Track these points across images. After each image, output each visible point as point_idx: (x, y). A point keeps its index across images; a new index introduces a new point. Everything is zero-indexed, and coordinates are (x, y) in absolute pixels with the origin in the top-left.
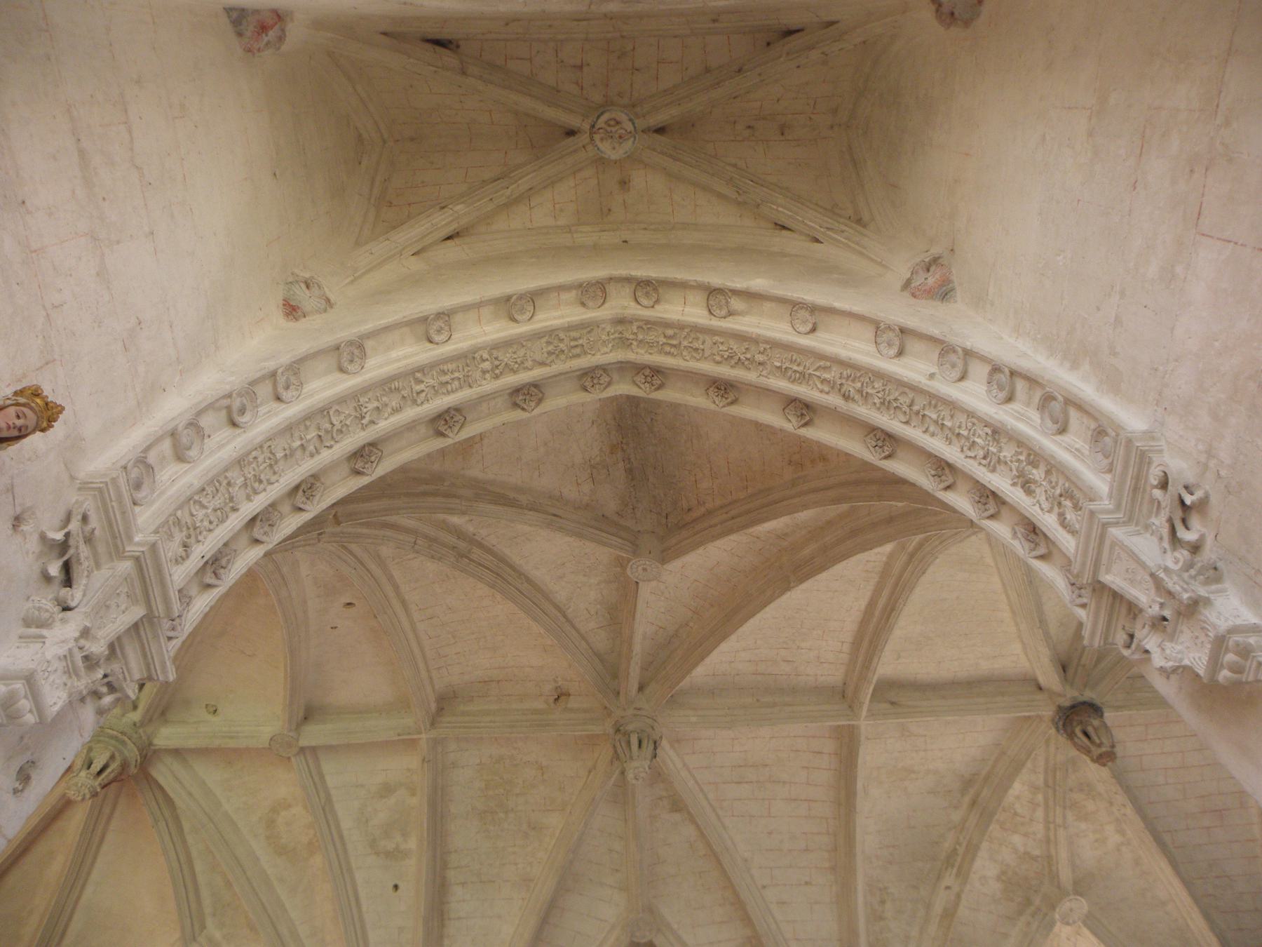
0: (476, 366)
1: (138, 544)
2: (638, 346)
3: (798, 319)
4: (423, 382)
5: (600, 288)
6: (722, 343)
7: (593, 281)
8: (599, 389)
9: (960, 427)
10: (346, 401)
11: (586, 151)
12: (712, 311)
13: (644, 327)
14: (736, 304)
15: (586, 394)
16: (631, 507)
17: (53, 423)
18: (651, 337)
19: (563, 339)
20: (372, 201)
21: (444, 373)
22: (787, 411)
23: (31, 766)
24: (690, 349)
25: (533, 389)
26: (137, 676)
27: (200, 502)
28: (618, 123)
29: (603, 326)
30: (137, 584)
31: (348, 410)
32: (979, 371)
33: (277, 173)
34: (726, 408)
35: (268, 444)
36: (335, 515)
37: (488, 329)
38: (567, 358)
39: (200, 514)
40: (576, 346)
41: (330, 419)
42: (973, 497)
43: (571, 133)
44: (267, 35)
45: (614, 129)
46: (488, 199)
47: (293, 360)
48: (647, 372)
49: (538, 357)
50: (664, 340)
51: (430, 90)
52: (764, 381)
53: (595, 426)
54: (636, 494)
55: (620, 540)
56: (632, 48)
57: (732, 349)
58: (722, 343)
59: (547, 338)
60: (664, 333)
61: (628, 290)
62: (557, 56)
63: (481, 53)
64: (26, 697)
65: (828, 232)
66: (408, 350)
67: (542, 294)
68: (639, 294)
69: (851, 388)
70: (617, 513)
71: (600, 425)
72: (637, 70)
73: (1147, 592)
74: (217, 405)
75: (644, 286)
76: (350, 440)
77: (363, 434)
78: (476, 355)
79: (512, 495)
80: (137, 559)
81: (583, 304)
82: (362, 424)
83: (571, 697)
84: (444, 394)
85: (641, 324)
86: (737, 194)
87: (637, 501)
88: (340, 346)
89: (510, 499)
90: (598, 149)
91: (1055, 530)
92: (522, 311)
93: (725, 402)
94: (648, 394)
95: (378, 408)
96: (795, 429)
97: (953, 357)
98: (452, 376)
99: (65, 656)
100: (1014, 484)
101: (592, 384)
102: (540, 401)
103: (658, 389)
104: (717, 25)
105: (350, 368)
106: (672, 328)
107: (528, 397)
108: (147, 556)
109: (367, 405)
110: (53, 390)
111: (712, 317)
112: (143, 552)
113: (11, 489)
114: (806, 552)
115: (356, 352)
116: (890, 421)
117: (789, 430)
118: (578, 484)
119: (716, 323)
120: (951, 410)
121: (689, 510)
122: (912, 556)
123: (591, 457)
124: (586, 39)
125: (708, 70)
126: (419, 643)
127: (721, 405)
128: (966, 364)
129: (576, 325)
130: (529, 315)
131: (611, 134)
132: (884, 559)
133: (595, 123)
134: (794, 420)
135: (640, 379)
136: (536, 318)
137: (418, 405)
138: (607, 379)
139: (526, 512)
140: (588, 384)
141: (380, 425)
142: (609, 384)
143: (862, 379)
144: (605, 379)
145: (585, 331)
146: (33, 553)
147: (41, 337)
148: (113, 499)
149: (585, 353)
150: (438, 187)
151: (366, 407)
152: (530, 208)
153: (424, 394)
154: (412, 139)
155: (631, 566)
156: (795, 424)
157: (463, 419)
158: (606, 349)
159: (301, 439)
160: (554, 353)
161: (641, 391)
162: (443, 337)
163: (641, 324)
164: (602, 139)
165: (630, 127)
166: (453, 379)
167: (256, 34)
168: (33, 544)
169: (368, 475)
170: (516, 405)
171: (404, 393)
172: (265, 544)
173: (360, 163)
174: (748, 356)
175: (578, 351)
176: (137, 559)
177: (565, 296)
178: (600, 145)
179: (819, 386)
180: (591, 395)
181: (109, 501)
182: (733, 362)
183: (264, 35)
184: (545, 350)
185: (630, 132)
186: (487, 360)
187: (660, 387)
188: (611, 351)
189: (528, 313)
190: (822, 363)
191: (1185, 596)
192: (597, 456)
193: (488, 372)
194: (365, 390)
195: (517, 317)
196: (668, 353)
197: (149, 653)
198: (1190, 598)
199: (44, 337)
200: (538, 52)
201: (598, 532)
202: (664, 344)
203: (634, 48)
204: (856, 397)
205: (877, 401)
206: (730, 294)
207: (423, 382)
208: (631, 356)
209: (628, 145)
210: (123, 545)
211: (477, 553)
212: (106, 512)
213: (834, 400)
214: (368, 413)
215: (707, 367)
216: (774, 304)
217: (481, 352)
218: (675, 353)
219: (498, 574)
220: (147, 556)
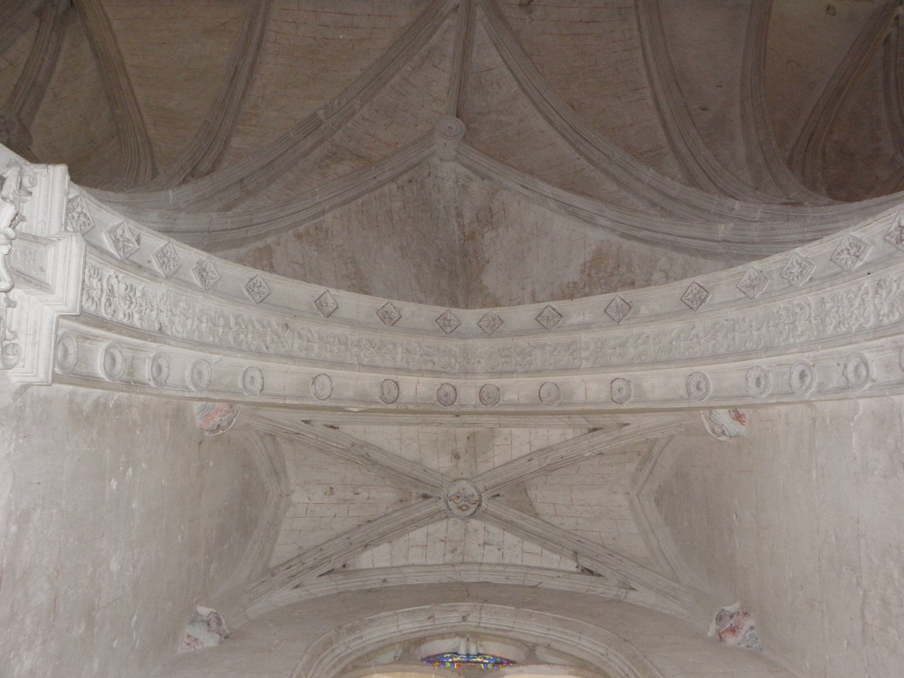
5: (484, 400)
12: (395, 385)
16: (459, 184)
28: (460, 508)
44: (731, 625)
45: (463, 503)
46: (564, 458)
53: (487, 259)
56: (446, 556)
62: (503, 552)
63: (560, 560)
68: (452, 395)
70: (471, 180)
71: (482, 259)
72: (443, 541)
83: (518, 3)
86: (370, 454)
87: (453, 188)
89: (564, 209)
91: (102, 263)
94: (449, 310)
96: (328, 290)
104: (383, 577)
111: (395, 380)
117: (333, 289)
126: (647, 67)
130: (545, 387)
150: (601, 463)
152: (530, 443)
162: (617, 384)
164: (473, 496)
165: (451, 504)
167: (739, 627)
183: (733, 626)
185: (451, 500)
189: (545, 388)
192: (486, 232)
200: (517, 557)
203: (444, 555)
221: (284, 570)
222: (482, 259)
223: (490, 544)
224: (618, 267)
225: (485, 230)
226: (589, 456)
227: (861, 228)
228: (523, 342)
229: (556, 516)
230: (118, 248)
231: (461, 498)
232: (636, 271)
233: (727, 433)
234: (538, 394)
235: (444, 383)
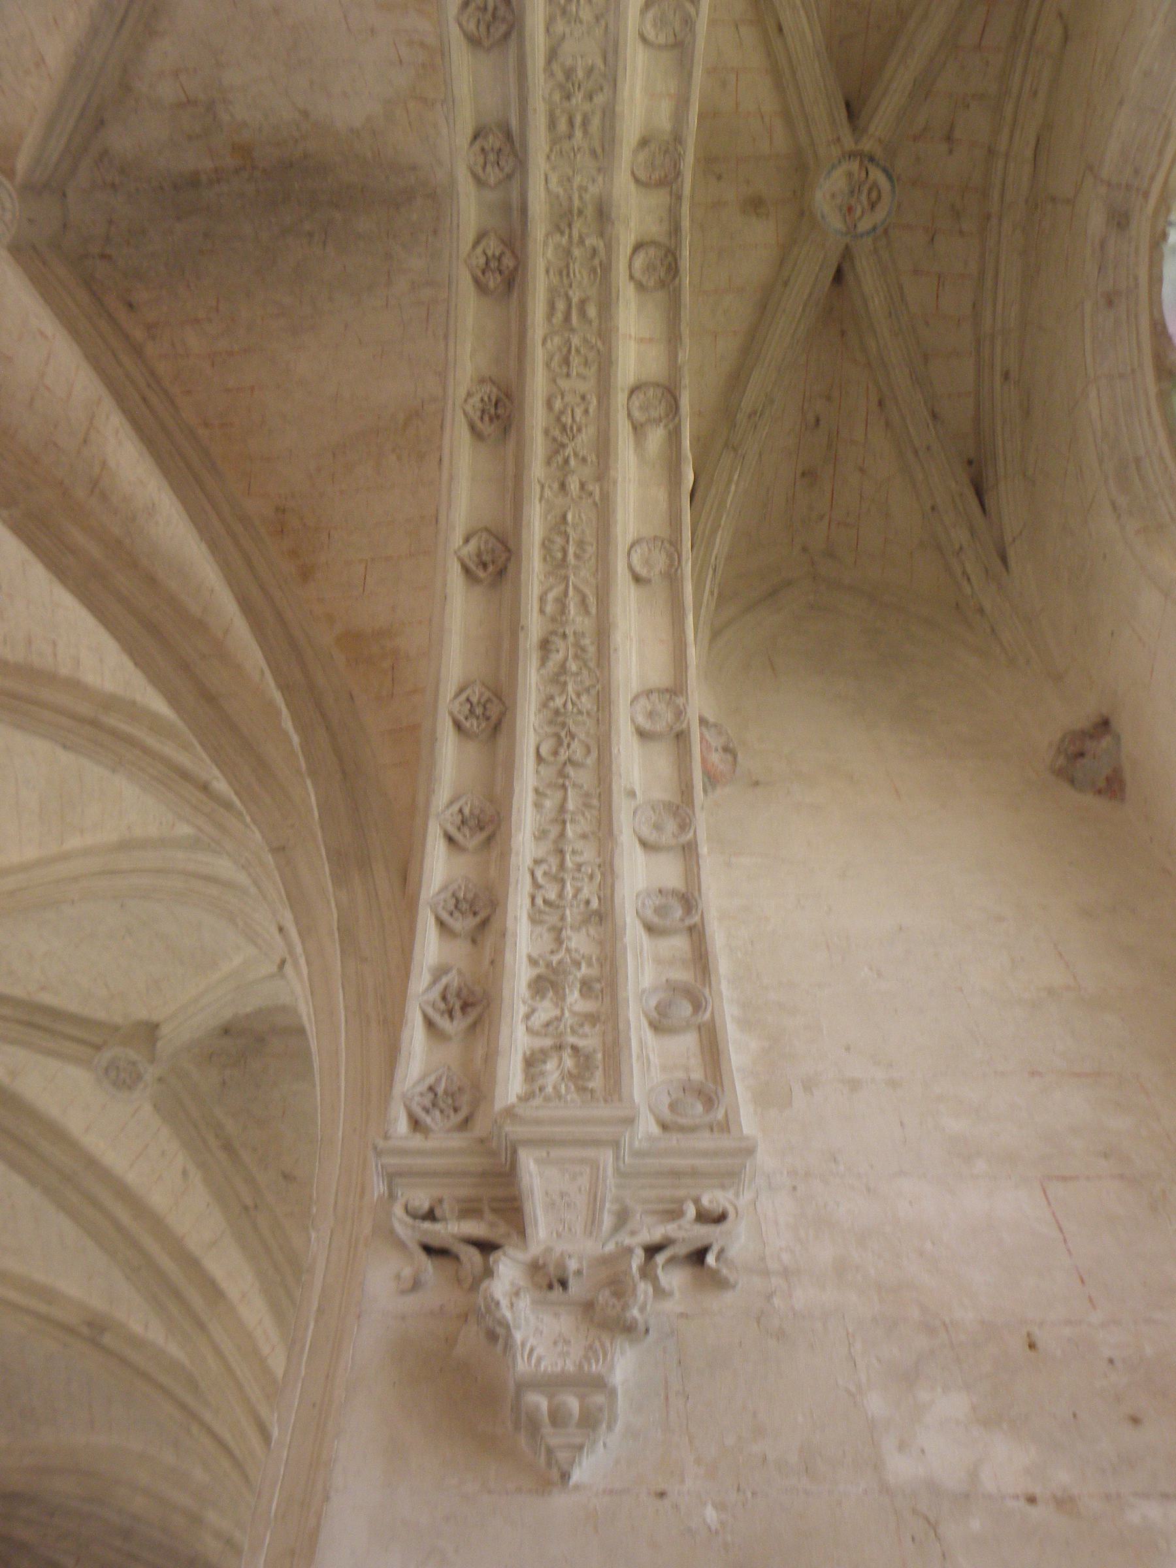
3: (650, 550)
6: (586, 411)
9: (574, 852)
13: (596, 262)
14: (656, 437)
18: (579, 270)
19: (591, 98)
22: (485, 535)
24: (565, 350)
25: (503, 28)
28: (873, 206)
29: (600, 179)
32: (669, 873)
34: (463, 420)
40: (571, 123)
42: (460, 887)
43: (852, 111)
45: (864, 197)
48: (508, 262)
49: (568, 47)
52: (533, 493)
57: (579, 430)
58: (586, 411)
59: (602, 67)
65: (711, 569)
68: (652, 251)
69: (562, 650)
73: (555, 1235)
81: (644, 142)
92: (661, 22)
93: (476, 417)
97: (671, 826)
100: (533, 962)
102: (474, 41)
103: (477, 281)
104: (998, 377)
106: (600, 315)
107: (488, 16)
114: (78, 537)
116: (532, 729)
119: (620, 399)
120: (593, 833)
121: (130, 305)
122: (94, 723)
124: (991, 151)
125: (926, 359)
127: (469, 408)
128: (669, 849)
129: (613, 127)
130: (651, 34)
132: (64, 671)
133: (878, 165)
134: (472, 546)
135: (493, 246)
136: (640, 47)
142: (479, 182)
143: (585, 672)
144: (493, 175)
145: (597, 144)
149: (554, 142)
156: (465, 552)
158: (554, 180)
161: (470, 245)
164: (850, 175)
174: (572, 462)
175: (562, 126)
178: (839, 173)
179: (551, 596)
180: (466, 146)
182: (557, 433)
190: (592, 600)
191: (635, 1312)
196: (552, 307)
198: (635, 1320)
202: (569, 300)
204: (550, 664)
205: (559, 702)
206: (671, 426)
208: (539, 228)
209: (836, 222)
213: (534, 626)
215: (538, 384)
216: (663, 506)
221: (972, 588)
223: (952, 128)
230: (533, 1070)
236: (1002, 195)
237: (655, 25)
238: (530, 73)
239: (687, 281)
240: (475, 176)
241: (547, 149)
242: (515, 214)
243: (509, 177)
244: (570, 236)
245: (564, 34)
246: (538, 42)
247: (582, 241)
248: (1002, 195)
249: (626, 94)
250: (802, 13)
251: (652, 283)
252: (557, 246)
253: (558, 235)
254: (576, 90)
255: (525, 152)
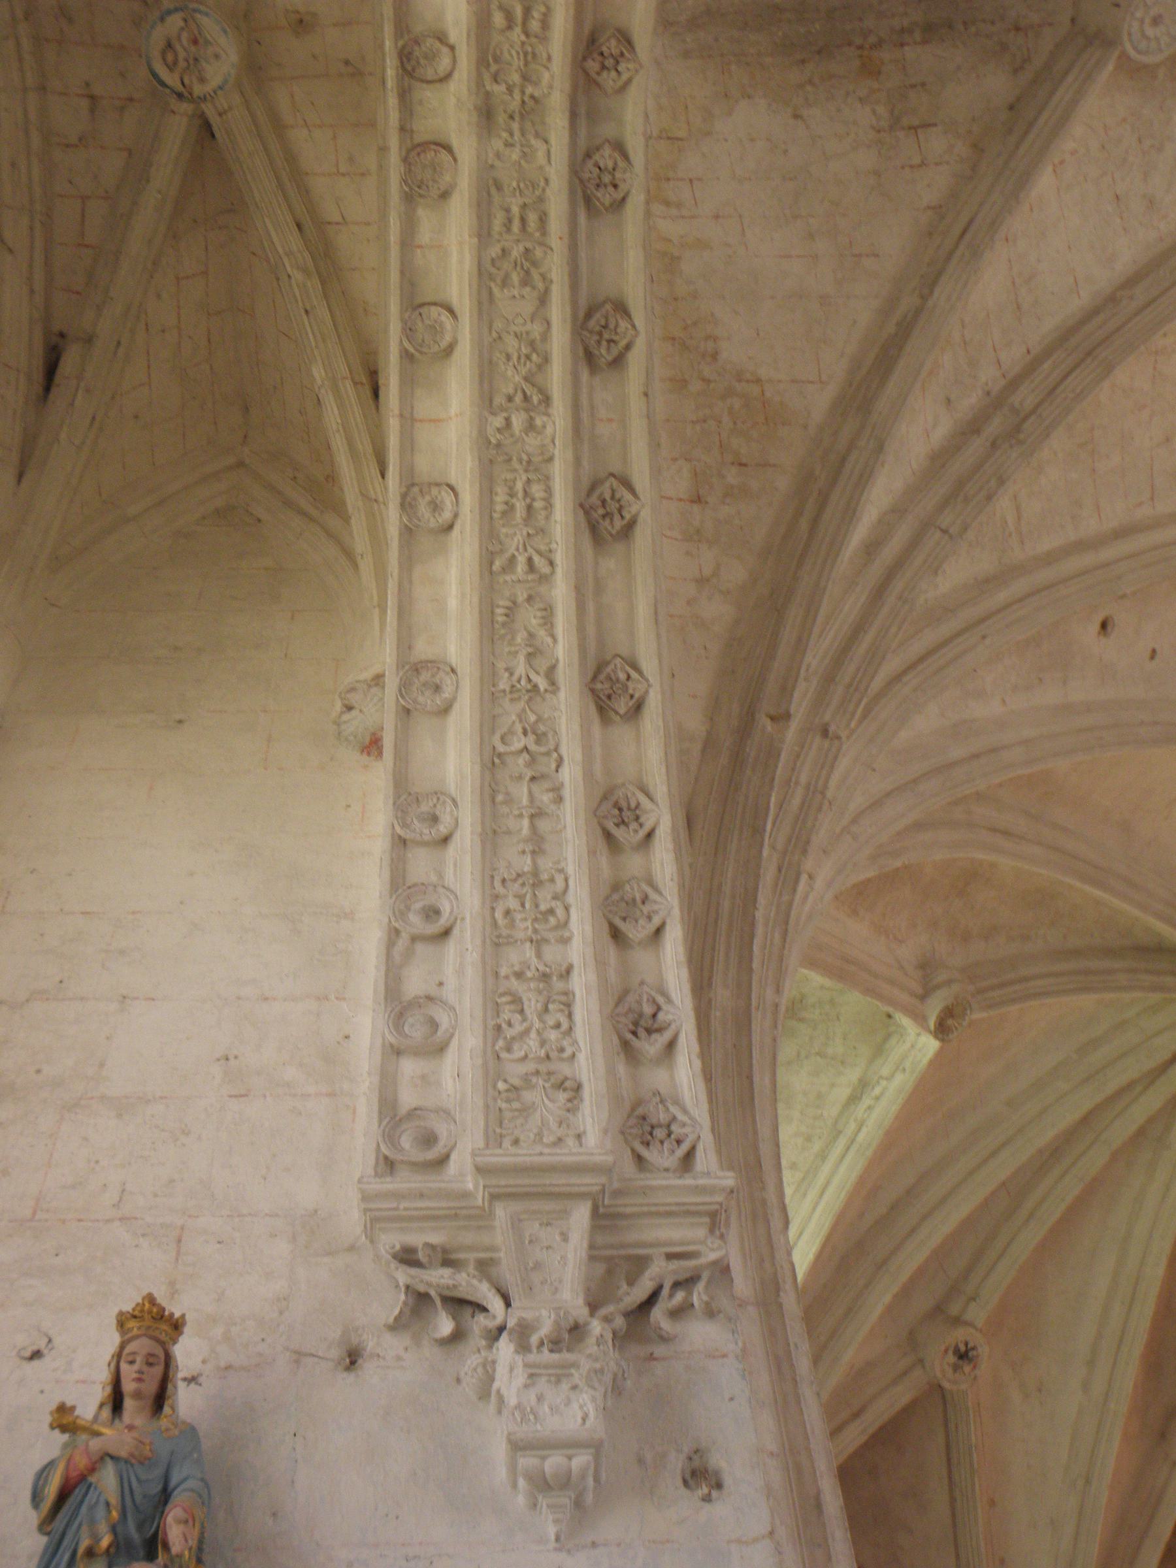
0: (516, 442)
1: (476, 1186)
2: (536, 84)
4: (514, 556)
5: (419, 154)
7: (402, 169)
8: (624, 172)
10: (494, 716)
11: (230, 108)
15: (629, 200)
17: (167, 1313)
19: (503, 250)
20: (314, 513)
21: (510, 508)
23: (701, 1457)
25: (592, 323)
26: (701, 1233)
27: (513, 1038)
28: (169, 45)
30: (535, 1205)
31: (510, 713)
33: (178, 717)
35: (497, 884)
36: (772, 718)
37: (454, 409)
38: (542, 244)
39: (532, 1042)
40: (523, 220)
41: (512, 753)
45: (182, 54)
46: (305, 317)
47: (391, 802)
48: (592, 65)
49: (528, 307)
50: (517, 34)
51: (142, 385)
54: (984, 21)
55: (1070, 78)
59: (492, 285)
60: (503, 31)
61: (427, 95)
64: (544, 1458)
66: (454, 573)
67: (412, 284)
71: (806, 99)
74: (397, 958)
75: (413, 62)
76: (563, 720)
77: (562, 695)
78: (494, 441)
79: (891, 328)
80: (494, 1197)
81: (445, 195)
82: (546, 691)
84: (547, 518)
85: (487, 77)
88: (404, 707)
90: (221, 88)
92: (436, 329)
95: (529, 654)
98: (520, 494)
99: (531, 1376)
101: (611, 189)
102: (622, 308)
103: (629, 42)
105: (447, 693)
106: (489, 14)
107: (606, 336)
108: (494, 1182)
109: (515, 677)
110: (219, 1242)
112: (484, 1187)
113: (299, 1356)
115: (425, 676)
118: (923, 164)
123: (873, 127)
124: (42, 89)
129: (479, 218)
130: (445, 317)
131: (191, 62)
135: (608, 80)
136: (455, 303)
137: (553, 573)
138: (607, 151)
139: (930, 303)
140: (605, 197)
141: (561, 658)
142: (620, 148)
144: (606, 157)
145: (496, 198)
146: (406, 1349)
147: (141, 1239)
148: (394, 1205)
149: (541, 200)
151: (519, 681)
153: (536, 558)
154: (246, 409)
155: (1139, 52)
157: (612, 479)
158: (541, 155)
159: (521, 816)
160: (527, 272)
161: (635, 82)
162: (447, 498)
163: (487, 77)
164: (202, 80)
166: (526, 492)
168: (394, 1345)
169: (647, 692)
170: (618, 362)
171: (521, 597)
172: (668, 921)
173: (259, 520)
175: (532, 218)
176: (494, 1197)
177: (425, 235)
178: (215, 82)
181: (396, 1213)
184: (516, 293)
185: (185, 20)
186: (508, 419)
187: (627, 40)
188: (546, 142)
189: (443, 318)
192: (874, 112)
193: (532, 419)
194: (488, 674)
195: (444, 344)
196: (545, 24)
197: (667, 1208)
199: (143, 1235)
201: (1031, 136)
207: (514, 556)
209: (210, 25)
210: (473, 1207)
211: (1025, 397)
212: (411, 1219)
214: (531, 677)
217: (490, 431)
218: (543, 9)
219: (1089, 354)
220: (494, 1182)
222: (806, 99)
223: (92, 111)
224: (741, 464)
225: (881, 110)
226: (313, 376)
227: (688, 1048)
228: (556, 266)
229: (177, 278)
231: (193, 49)
232: (726, 507)
233: (346, 717)
234: (428, 300)
235: (457, 52)
236: (18, 44)
237: (441, 324)
238: (566, 278)
239: (388, 44)
240: (625, 156)
241: (548, 192)
242: (582, 110)
243: (588, 155)
244: (523, 93)
245: (532, 322)
246: (558, 313)
247: (510, 90)
248: (18, 44)
249: (467, 256)
250: (280, 250)
251: (429, 42)
252: (536, 84)
253: (536, 94)
254: (519, 260)
255: (571, 183)
